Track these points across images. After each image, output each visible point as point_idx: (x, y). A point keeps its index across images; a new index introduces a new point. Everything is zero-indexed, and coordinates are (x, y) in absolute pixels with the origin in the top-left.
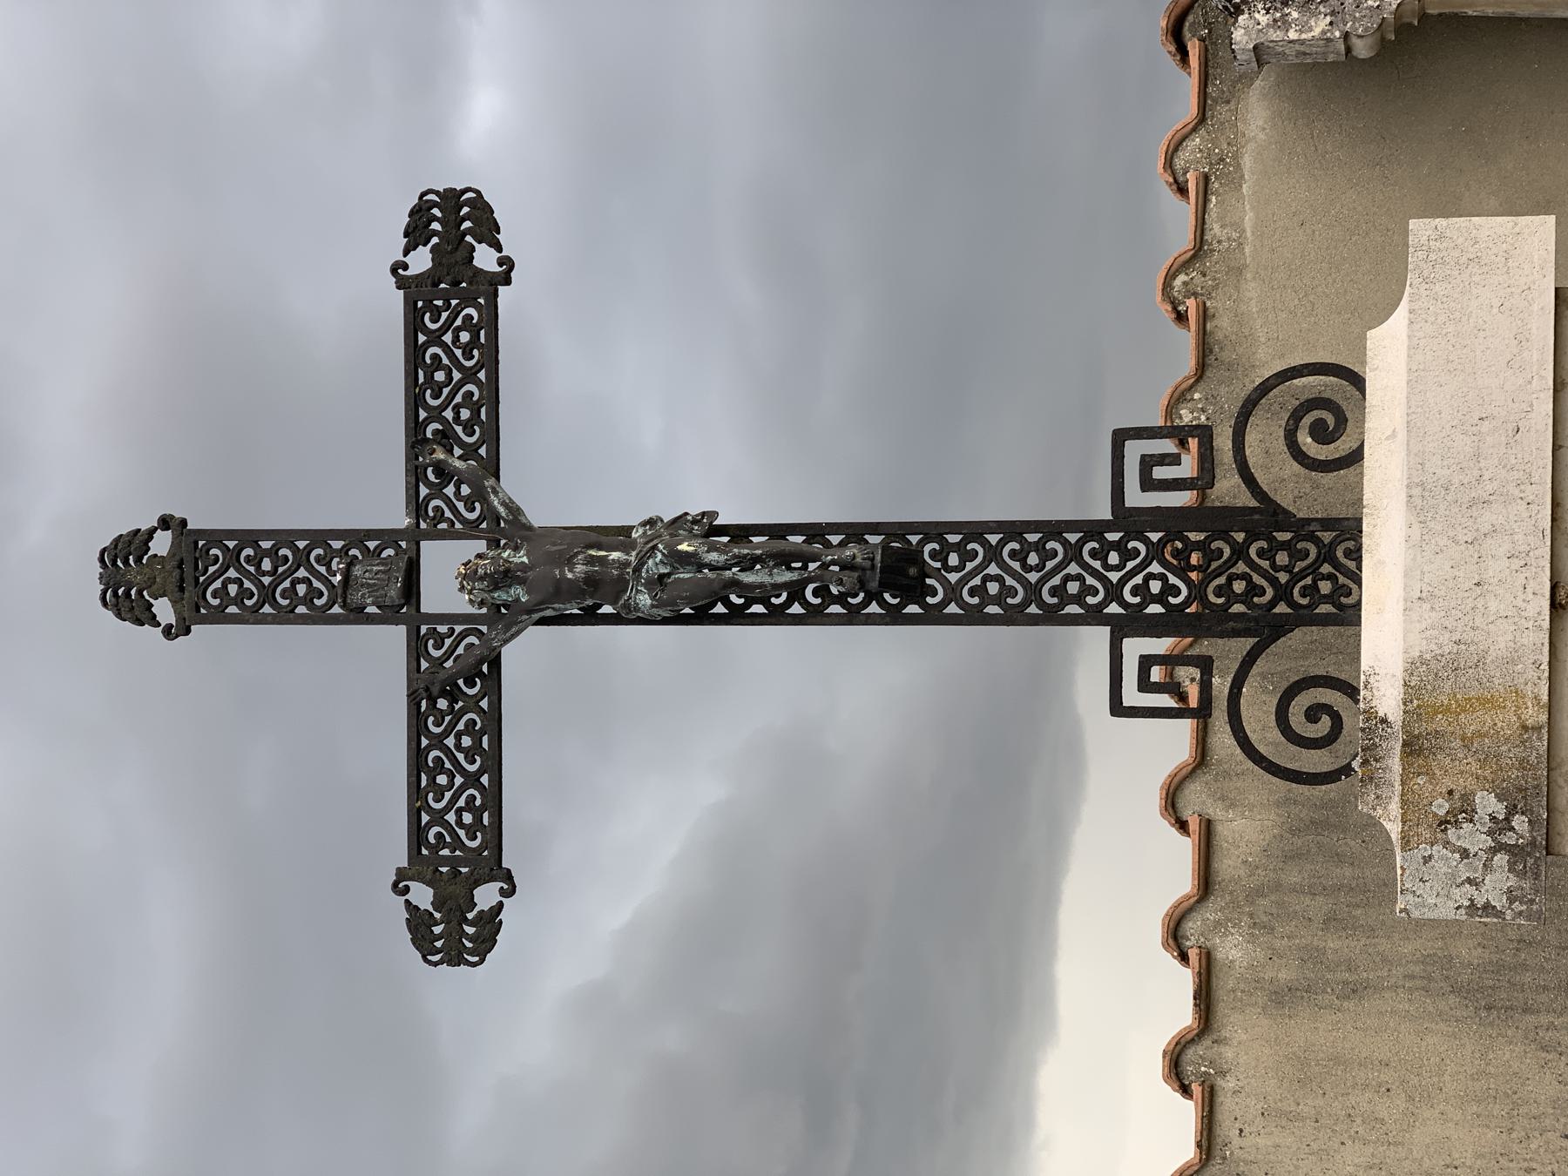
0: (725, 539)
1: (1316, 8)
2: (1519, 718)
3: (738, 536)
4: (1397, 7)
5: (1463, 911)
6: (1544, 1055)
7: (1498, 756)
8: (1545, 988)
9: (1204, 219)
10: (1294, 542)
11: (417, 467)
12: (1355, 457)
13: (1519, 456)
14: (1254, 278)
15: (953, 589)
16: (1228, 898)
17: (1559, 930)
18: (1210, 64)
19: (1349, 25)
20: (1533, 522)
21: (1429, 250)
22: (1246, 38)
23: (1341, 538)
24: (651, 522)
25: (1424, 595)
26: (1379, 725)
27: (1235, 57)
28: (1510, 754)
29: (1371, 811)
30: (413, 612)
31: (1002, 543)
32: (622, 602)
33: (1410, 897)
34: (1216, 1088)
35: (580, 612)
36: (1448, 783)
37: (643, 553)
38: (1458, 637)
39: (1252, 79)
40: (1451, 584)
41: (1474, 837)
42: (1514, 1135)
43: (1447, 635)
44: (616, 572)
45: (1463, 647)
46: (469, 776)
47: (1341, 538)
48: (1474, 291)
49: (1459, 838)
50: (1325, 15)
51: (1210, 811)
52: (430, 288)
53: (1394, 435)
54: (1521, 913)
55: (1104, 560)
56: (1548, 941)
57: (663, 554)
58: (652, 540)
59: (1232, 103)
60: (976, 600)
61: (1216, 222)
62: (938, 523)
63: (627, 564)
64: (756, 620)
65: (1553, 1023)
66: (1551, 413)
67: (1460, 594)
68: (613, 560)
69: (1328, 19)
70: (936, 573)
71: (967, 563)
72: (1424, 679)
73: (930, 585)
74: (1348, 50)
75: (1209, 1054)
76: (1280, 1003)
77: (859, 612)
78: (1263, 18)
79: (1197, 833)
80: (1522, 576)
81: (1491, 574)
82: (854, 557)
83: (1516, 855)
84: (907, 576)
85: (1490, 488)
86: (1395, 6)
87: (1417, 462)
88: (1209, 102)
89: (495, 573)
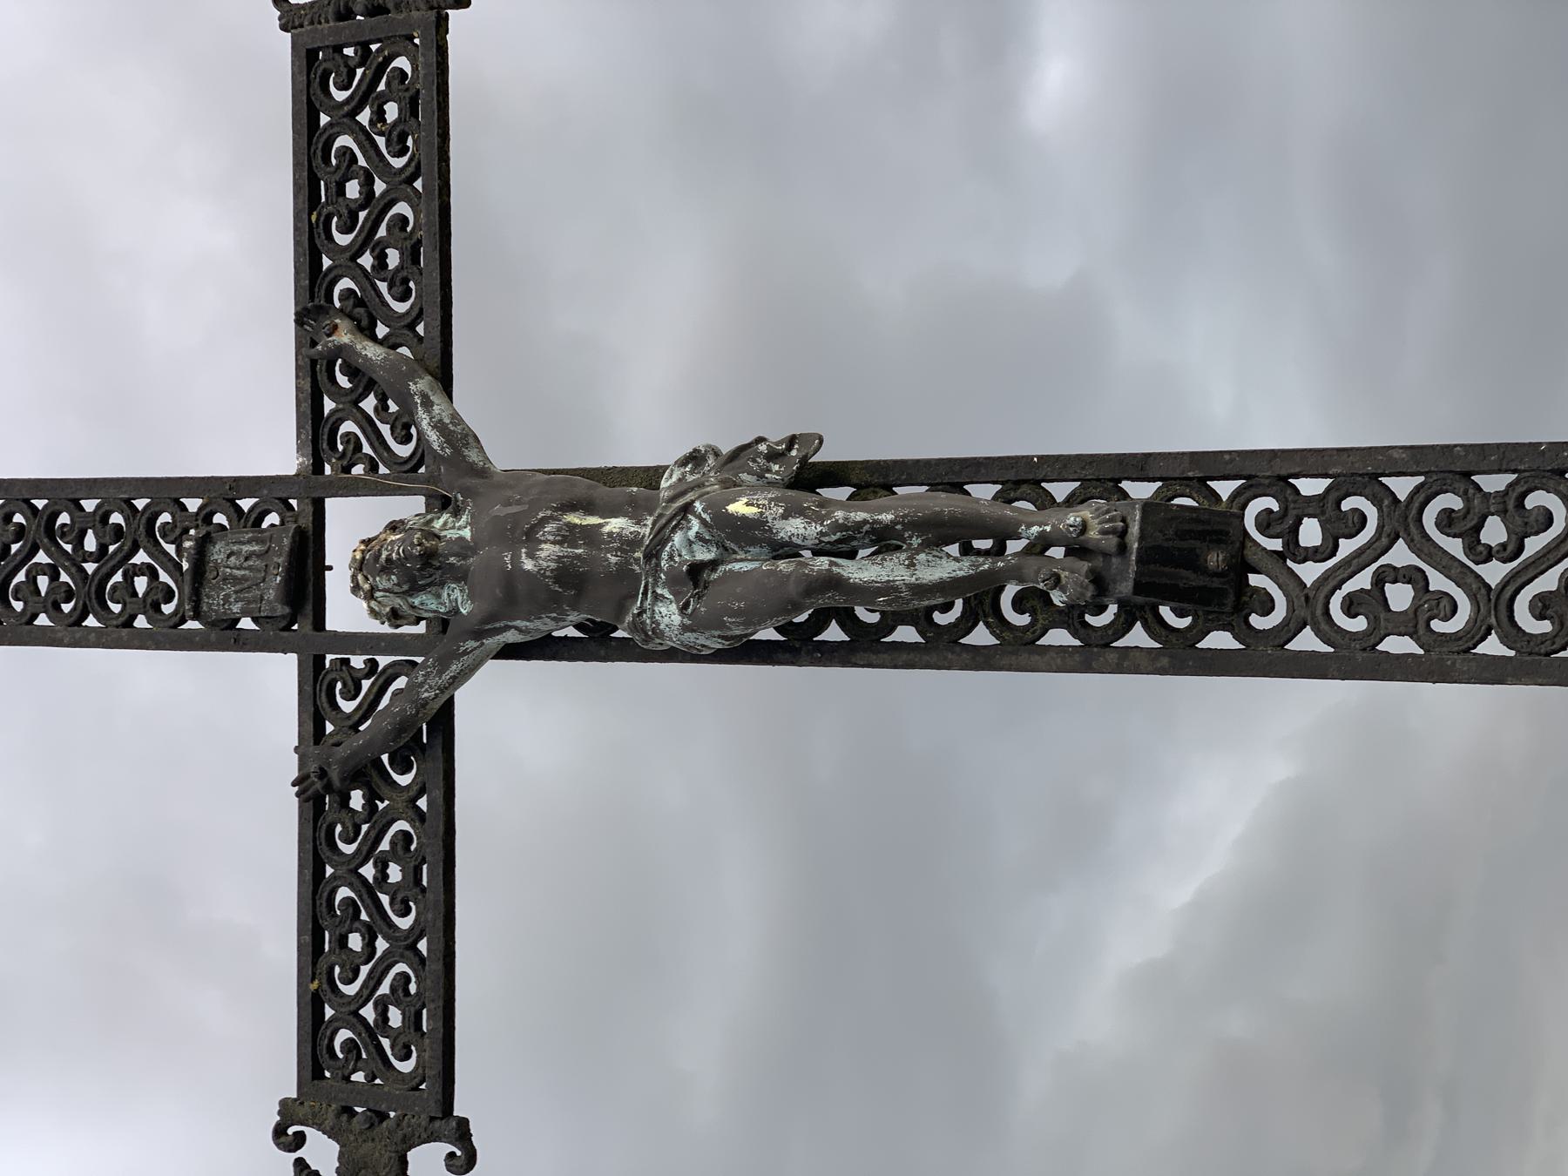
0: (843, 493)
3: (868, 486)
11: (314, 362)
15: (1307, 598)
24: (695, 459)
30: (308, 628)
31: (1421, 497)
32: (629, 618)
35: (577, 634)
37: (663, 521)
44: (613, 560)
46: (397, 939)
52: (332, 24)
55: (1471, 537)
57: (703, 522)
58: (683, 493)
60: (1359, 624)
62: (1274, 454)
63: (633, 543)
64: (904, 657)
68: (610, 534)
70: (1269, 563)
71: (1341, 541)
73: (1256, 590)
77: (1107, 645)
82: (1084, 527)
84: (1201, 569)
89: (406, 558)
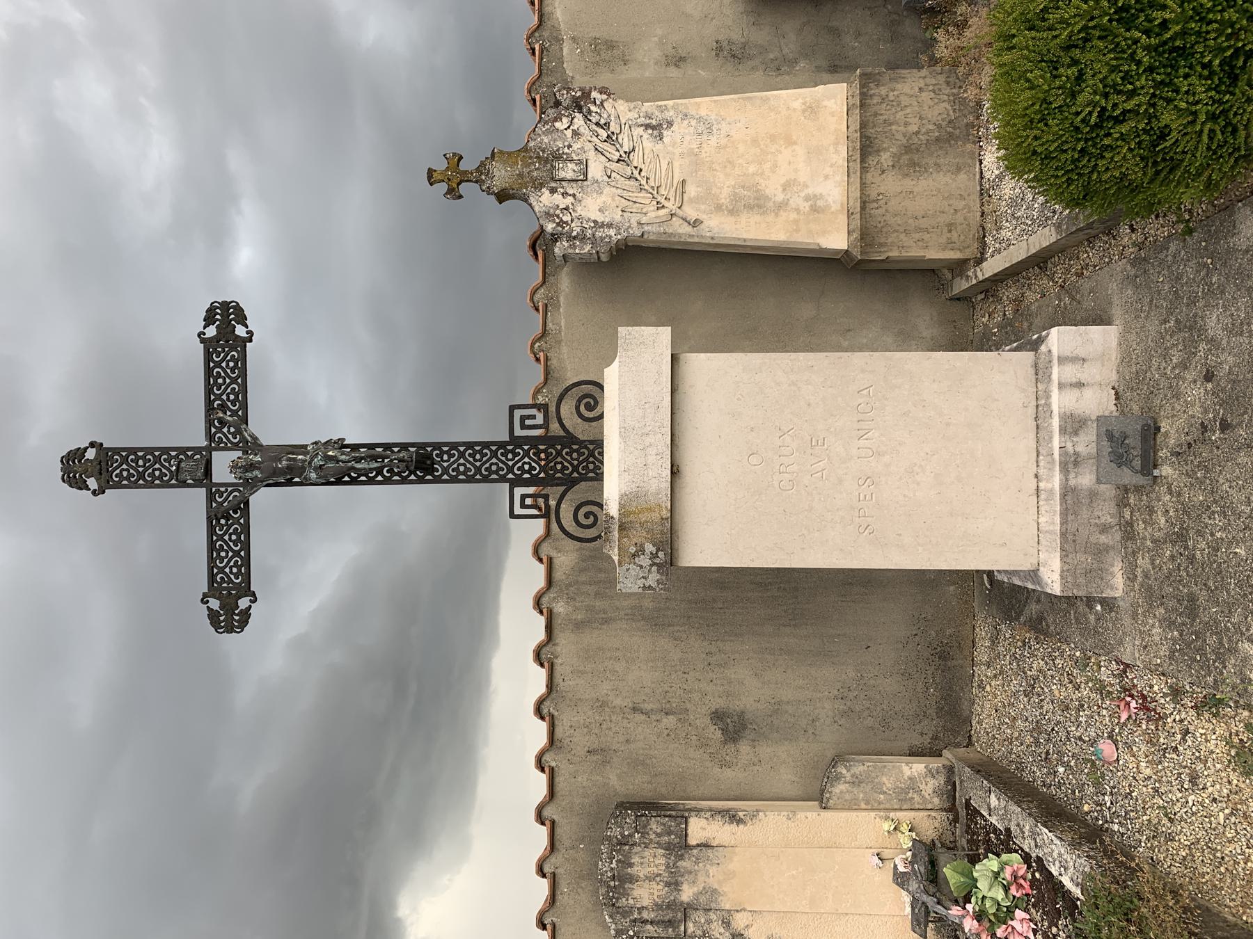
12: (601, 417)
28: (657, 529)
33: (622, 585)
36: (635, 540)
41: (644, 561)
53: (615, 408)
74: (599, 258)
76: (578, 628)
78: (566, 244)
87: (623, 419)
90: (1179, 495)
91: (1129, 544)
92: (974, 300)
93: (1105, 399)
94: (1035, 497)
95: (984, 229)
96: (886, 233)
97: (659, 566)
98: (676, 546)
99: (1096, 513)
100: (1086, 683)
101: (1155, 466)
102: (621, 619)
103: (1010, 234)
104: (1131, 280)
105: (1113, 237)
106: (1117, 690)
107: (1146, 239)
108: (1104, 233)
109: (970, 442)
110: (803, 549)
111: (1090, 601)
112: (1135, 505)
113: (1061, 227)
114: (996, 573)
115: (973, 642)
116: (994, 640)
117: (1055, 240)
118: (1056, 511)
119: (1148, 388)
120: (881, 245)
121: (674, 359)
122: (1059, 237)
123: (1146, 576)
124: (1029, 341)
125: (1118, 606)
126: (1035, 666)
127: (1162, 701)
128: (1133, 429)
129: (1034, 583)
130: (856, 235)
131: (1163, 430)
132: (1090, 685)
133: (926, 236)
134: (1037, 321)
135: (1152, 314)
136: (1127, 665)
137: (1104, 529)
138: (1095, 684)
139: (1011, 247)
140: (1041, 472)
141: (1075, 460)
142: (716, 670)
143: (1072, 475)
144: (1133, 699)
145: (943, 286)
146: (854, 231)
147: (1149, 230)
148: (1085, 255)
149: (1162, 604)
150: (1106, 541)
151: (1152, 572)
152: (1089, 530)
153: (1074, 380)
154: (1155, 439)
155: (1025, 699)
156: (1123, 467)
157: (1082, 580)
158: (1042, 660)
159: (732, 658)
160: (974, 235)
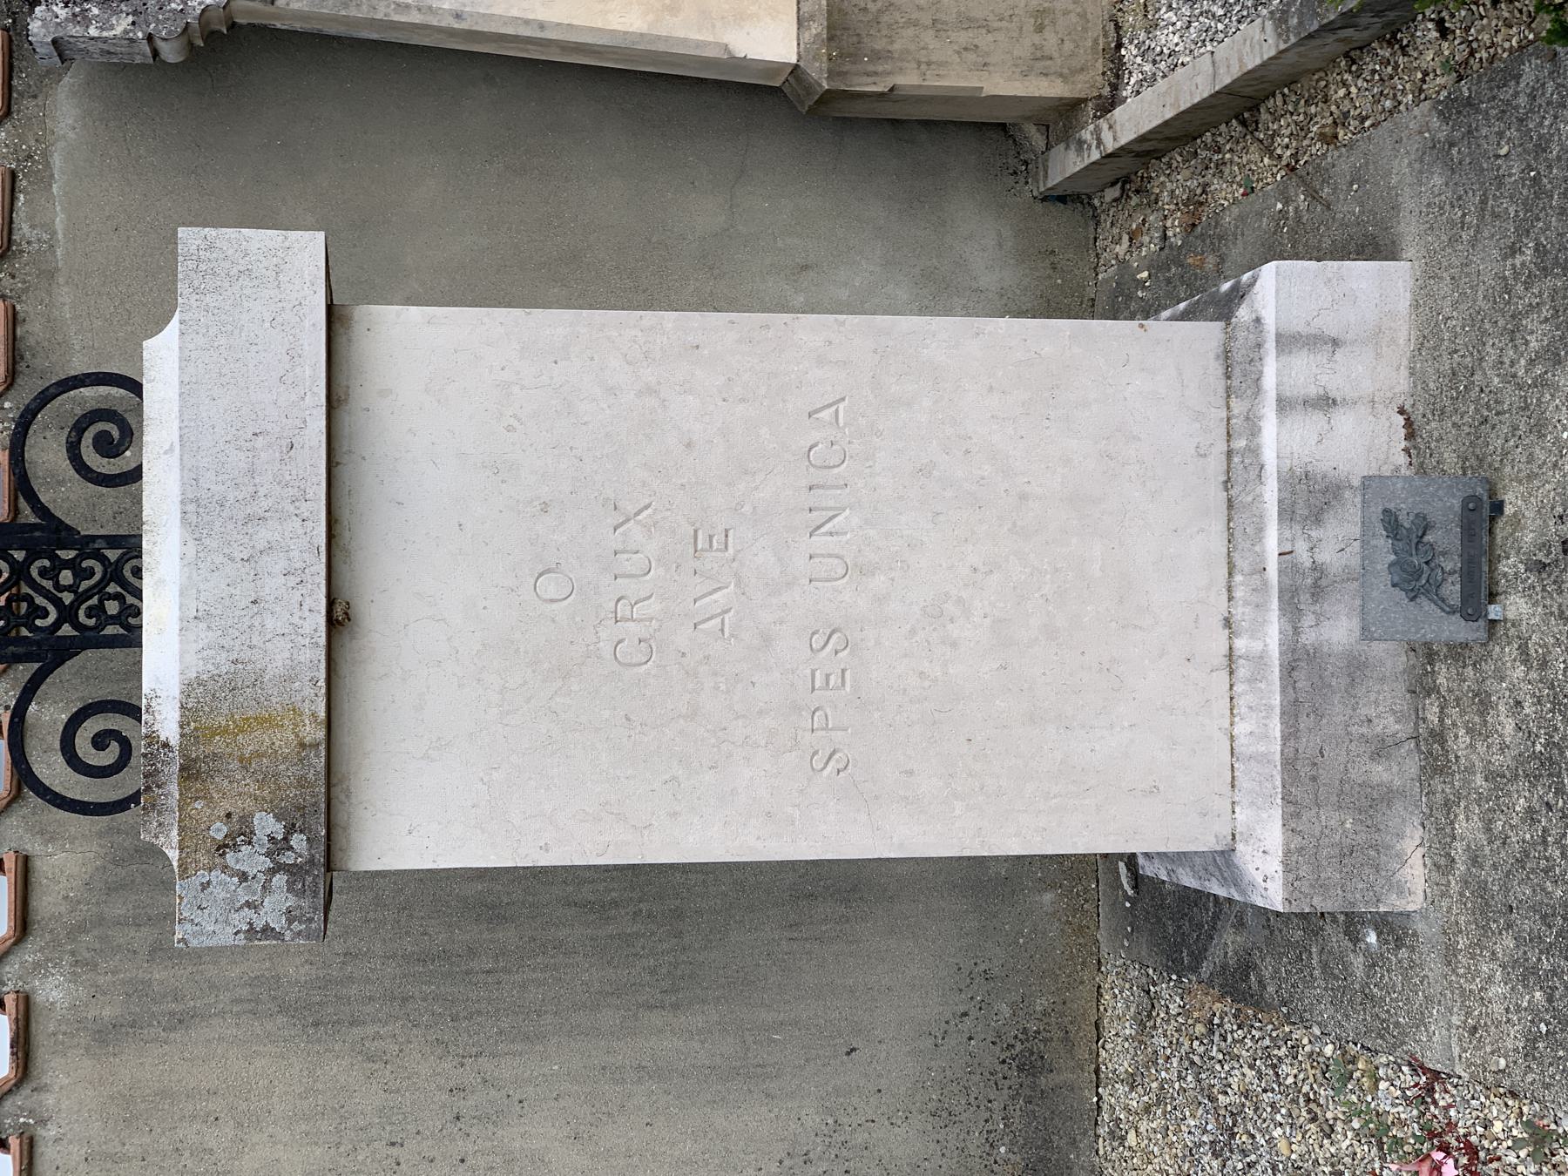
1: (118, 6)
2: (297, 736)
4: (201, 14)
5: (242, 936)
6: (370, 1065)
7: (276, 775)
8: (371, 999)
9: (11, 218)
10: (78, 560)
12: (136, 475)
13: (294, 472)
14: (67, 283)
16: (48, 937)
17: (384, 939)
18: (15, 55)
19: (152, 26)
20: (308, 539)
21: (199, 260)
22: (44, 30)
23: (128, 556)
25: (200, 614)
26: (161, 750)
27: (34, 50)
28: (289, 773)
29: (154, 840)
33: (188, 926)
34: (36, 1138)
36: (226, 806)
38: (235, 656)
39: (60, 75)
40: (227, 602)
41: (252, 860)
42: (342, 1149)
43: (224, 655)
45: (240, 666)
47: (128, 556)
48: (245, 304)
49: (237, 862)
50: (128, 14)
51: (28, 846)
53: (171, 449)
54: (299, 933)
56: (373, 951)
59: (40, 98)
61: (25, 222)
65: (378, 1032)
66: (324, 430)
67: (237, 613)
69: (130, 18)
72: (202, 700)
74: (155, 53)
75: (28, 1104)
76: (103, 1042)
78: (62, 13)
79: (13, 870)
80: (298, 594)
81: (267, 591)
83: (295, 874)
85: (265, 504)
86: (199, 12)
87: (191, 478)
88: (15, 95)
90: (1544, 664)
91: (1437, 783)
92: (1096, 202)
93: (1385, 438)
94: (1224, 675)
95: (1118, 27)
96: (889, 26)
97: (293, 871)
98: (340, 817)
99: (1363, 711)
100: (1348, 1121)
101: (1492, 597)
102: (222, 1014)
103: (1176, 39)
104: (1439, 151)
105: (1403, 48)
106: (1414, 1135)
107: (1472, 53)
108: (1381, 39)
109: (1074, 541)
110: (675, 814)
111: (1352, 924)
112: (1450, 691)
113: (1286, 21)
114: (1141, 861)
115: (1097, 1029)
116: (1145, 1020)
117: (1273, 53)
118: (1271, 708)
119: (1477, 410)
120: (877, 56)
121: (335, 317)
122: (1282, 46)
123: (1475, 861)
124: (1213, 296)
125: (1415, 934)
126: (1234, 1081)
127: (1512, 1159)
128: (1445, 507)
129: (1224, 882)
130: (817, 28)
131: (1509, 510)
132: (1356, 1124)
133: (984, 40)
134: (1236, 252)
135: (1486, 234)
136: (1436, 1075)
137: (1381, 749)
138: (1367, 1122)
139: (1179, 70)
140: (1239, 611)
141: (1316, 585)
142: (474, 1131)
143: (1308, 621)
144: (1448, 1154)
145: (1026, 166)
146: (812, 18)
147: (1479, 32)
148: (1342, 92)
149: (1509, 926)
150: (1386, 777)
151: (1487, 849)
152: (1348, 752)
153: (1313, 391)
154: (1491, 532)
155: (1215, 1163)
156: (1423, 600)
157: (1331, 874)
158: (1251, 1067)
159: (517, 1097)
160: (1096, 41)
